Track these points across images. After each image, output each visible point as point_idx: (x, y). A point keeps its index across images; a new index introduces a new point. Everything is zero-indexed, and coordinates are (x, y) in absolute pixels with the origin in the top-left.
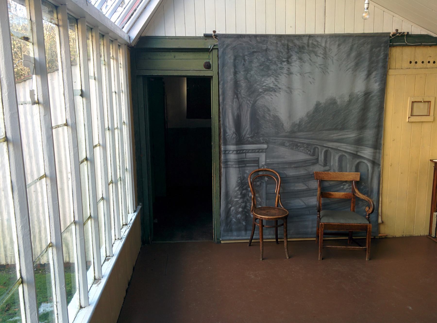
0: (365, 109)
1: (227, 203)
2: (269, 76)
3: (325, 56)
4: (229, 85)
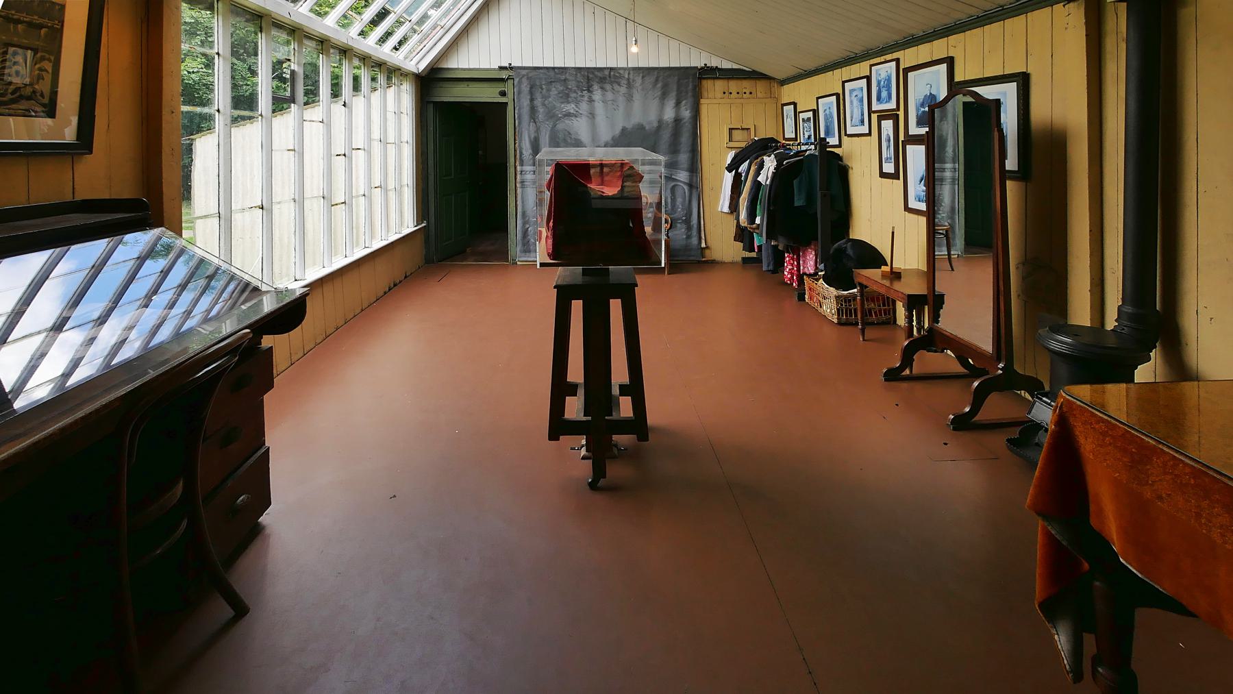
0: (676, 134)
1: (524, 223)
2: (568, 102)
3: (630, 85)
4: (526, 111)
